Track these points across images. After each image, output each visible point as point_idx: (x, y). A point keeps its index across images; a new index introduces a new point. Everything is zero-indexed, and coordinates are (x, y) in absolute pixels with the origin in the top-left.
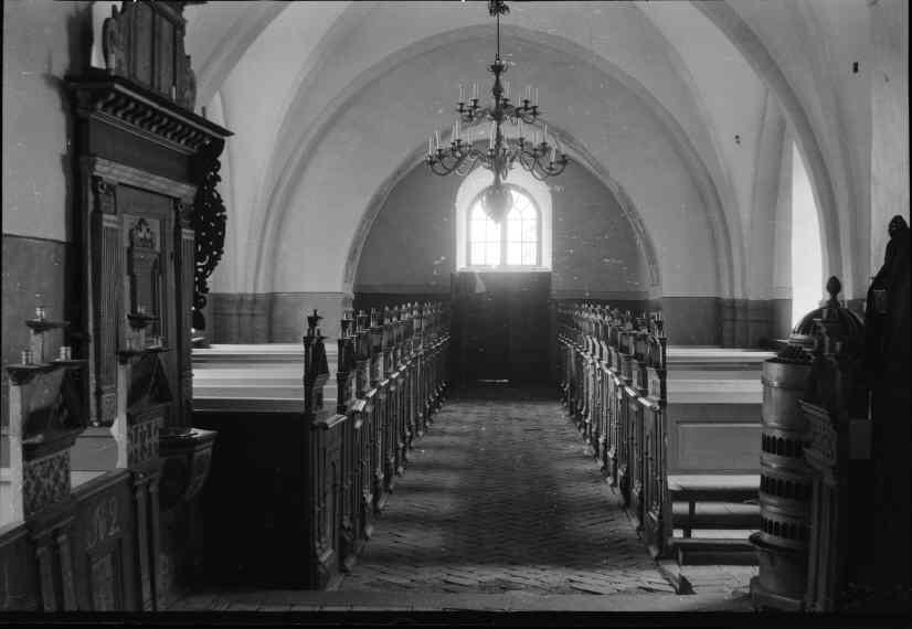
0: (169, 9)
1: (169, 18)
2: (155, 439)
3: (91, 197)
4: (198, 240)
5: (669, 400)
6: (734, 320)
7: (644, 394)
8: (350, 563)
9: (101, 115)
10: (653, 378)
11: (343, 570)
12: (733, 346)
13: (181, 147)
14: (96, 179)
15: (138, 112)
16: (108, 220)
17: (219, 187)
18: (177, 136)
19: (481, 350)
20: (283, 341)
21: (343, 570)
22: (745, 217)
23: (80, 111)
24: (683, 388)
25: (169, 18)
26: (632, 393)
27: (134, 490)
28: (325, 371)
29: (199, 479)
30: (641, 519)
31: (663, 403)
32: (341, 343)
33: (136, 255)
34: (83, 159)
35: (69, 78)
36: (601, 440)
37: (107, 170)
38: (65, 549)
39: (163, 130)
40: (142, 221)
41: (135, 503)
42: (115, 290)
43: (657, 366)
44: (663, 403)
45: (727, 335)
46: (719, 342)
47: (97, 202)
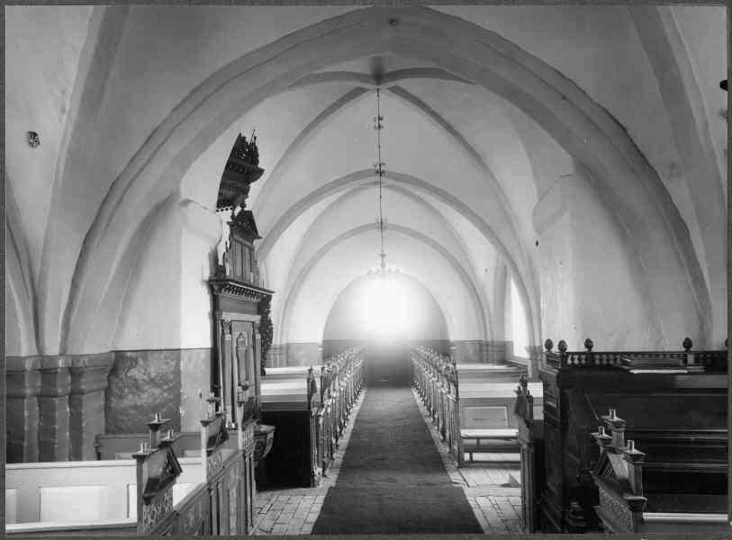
0: (248, 244)
1: (247, 247)
2: (252, 434)
3: (221, 328)
4: (262, 337)
5: (461, 396)
6: (488, 351)
7: (449, 392)
8: (327, 472)
9: (226, 297)
10: (452, 387)
11: (324, 476)
12: (487, 362)
13: (255, 300)
14: (222, 321)
15: (240, 291)
16: (228, 337)
17: (270, 315)
18: (253, 296)
19: (357, 140)
20: (293, 365)
21: (324, 476)
22: (492, 308)
23: (215, 293)
24: (469, 389)
25: (247, 247)
26: (444, 391)
27: (245, 458)
28: (316, 391)
29: (269, 448)
30: (450, 447)
31: (457, 399)
32: (321, 378)
33: (240, 349)
34: (217, 313)
35: (210, 281)
36: (432, 409)
37: (227, 317)
38: (221, 490)
39: (247, 295)
40: (241, 334)
41: (245, 464)
42: (231, 370)
43: (454, 382)
44: (457, 399)
45: (485, 358)
46: (481, 361)
47: (223, 331)
